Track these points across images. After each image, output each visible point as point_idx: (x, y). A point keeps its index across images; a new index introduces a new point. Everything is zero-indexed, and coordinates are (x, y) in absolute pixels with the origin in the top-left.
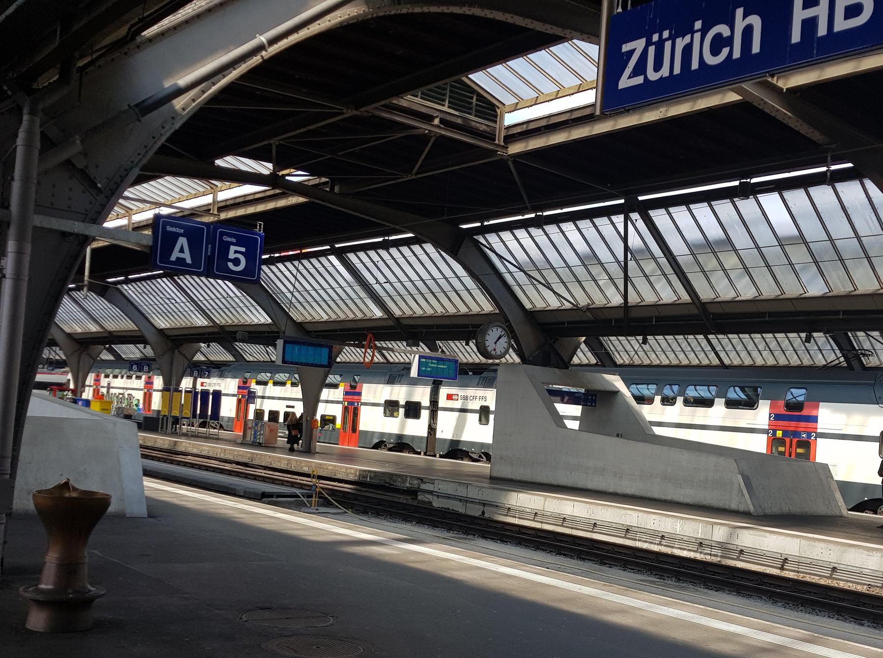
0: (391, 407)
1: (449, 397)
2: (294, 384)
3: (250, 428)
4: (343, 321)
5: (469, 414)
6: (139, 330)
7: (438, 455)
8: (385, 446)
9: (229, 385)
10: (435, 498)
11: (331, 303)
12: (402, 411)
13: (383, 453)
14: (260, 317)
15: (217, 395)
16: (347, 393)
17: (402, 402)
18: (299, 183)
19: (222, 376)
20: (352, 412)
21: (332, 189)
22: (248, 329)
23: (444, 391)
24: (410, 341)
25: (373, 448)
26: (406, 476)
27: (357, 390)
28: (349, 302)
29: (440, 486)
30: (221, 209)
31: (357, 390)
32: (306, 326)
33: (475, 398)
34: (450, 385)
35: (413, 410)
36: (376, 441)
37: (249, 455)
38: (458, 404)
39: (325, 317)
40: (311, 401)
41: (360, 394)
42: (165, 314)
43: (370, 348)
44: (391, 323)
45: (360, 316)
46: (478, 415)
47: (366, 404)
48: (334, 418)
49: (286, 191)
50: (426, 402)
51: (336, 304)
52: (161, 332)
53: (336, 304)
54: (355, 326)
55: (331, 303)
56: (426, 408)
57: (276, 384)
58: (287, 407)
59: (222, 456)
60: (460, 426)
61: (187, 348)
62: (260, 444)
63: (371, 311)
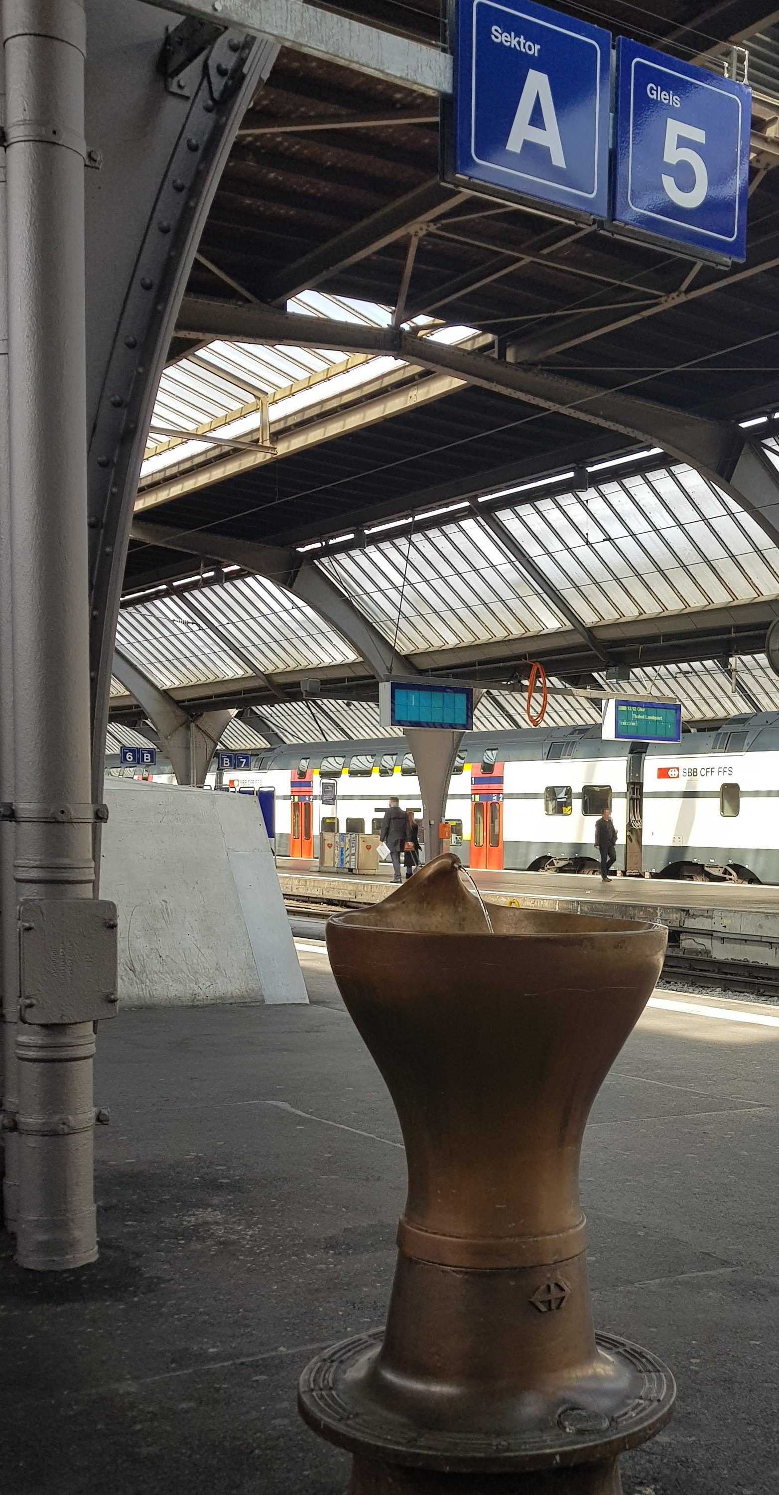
0: (557, 801)
1: (663, 773)
2: (406, 772)
3: (330, 846)
4: (487, 645)
5: (698, 801)
6: (132, 695)
7: (647, 875)
8: (552, 864)
9: (278, 780)
10: (717, 943)
11: (464, 613)
12: (577, 804)
13: (547, 875)
14: (337, 652)
15: (266, 800)
16: (477, 780)
17: (577, 789)
18: (455, 349)
19: (262, 767)
20: (488, 810)
21: (502, 354)
22: (323, 676)
23: (651, 764)
24: (612, 670)
25: (529, 869)
26: (655, 908)
27: (495, 773)
28: (497, 607)
29: (726, 922)
30: (276, 436)
31: (495, 773)
32: (416, 661)
33: (709, 771)
34: (664, 751)
35: (596, 800)
36: (534, 857)
37: (350, 887)
38: (679, 785)
39: (452, 641)
40: (436, 795)
41: (500, 780)
42: (171, 663)
43: (538, 690)
44: (579, 639)
45: (517, 631)
46: (717, 801)
47: (511, 796)
48: (459, 824)
49: (430, 366)
50: (619, 785)
51: (474, 613)
52: (166, 694)
53: (474, 613)
54: (482, 657)
55: (464, 613)
56: (619, 795)
57: (353, 774)
58: (377, 810)
59: (302, 892)
60: (685, 822)
61: (209, 720)
62: (351, 870)
63: (538, 620)
